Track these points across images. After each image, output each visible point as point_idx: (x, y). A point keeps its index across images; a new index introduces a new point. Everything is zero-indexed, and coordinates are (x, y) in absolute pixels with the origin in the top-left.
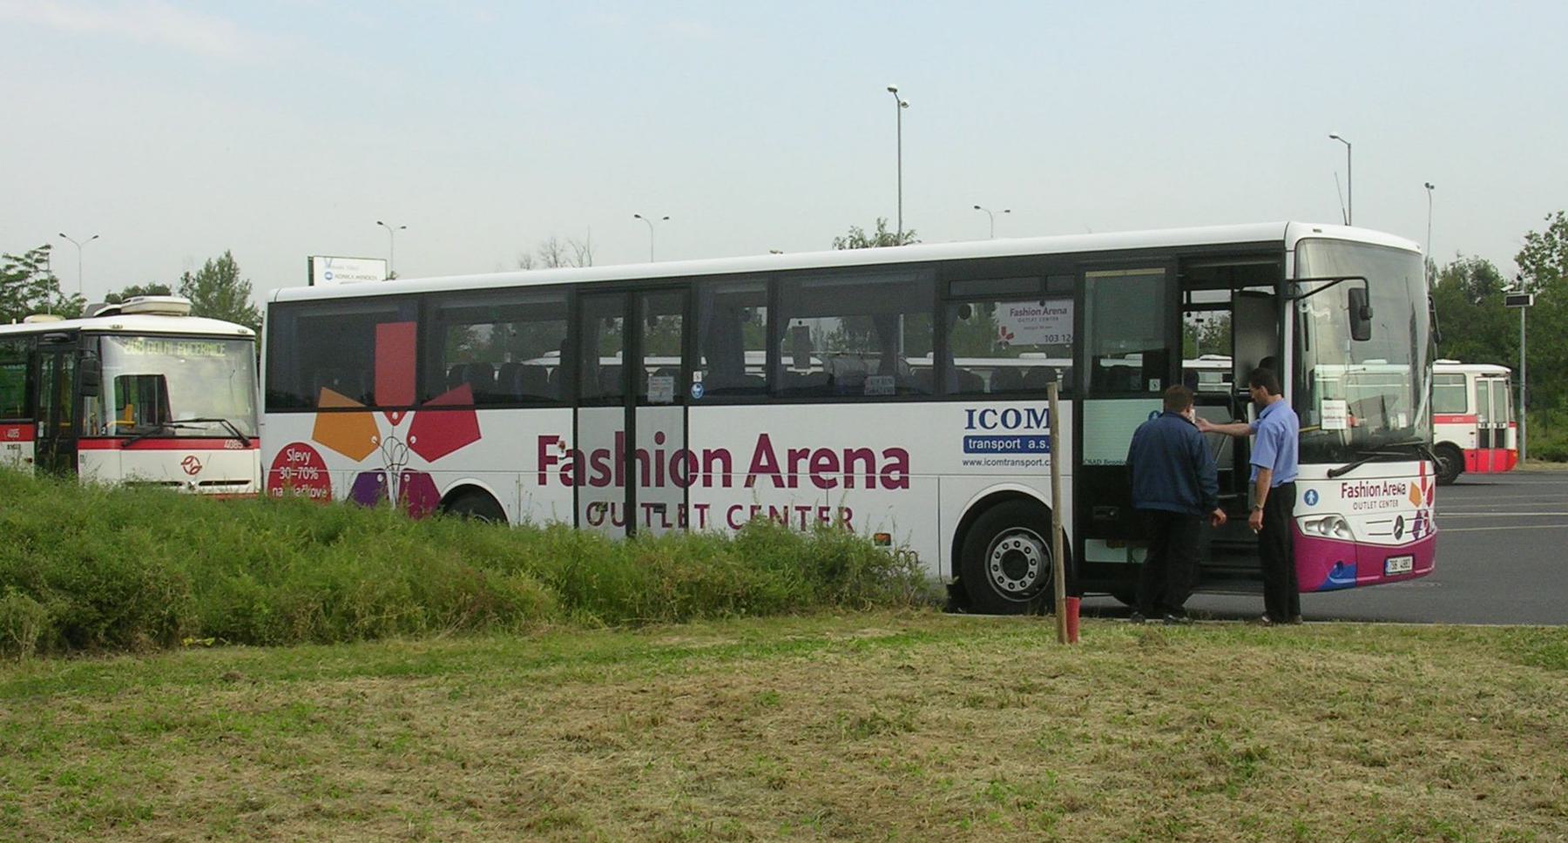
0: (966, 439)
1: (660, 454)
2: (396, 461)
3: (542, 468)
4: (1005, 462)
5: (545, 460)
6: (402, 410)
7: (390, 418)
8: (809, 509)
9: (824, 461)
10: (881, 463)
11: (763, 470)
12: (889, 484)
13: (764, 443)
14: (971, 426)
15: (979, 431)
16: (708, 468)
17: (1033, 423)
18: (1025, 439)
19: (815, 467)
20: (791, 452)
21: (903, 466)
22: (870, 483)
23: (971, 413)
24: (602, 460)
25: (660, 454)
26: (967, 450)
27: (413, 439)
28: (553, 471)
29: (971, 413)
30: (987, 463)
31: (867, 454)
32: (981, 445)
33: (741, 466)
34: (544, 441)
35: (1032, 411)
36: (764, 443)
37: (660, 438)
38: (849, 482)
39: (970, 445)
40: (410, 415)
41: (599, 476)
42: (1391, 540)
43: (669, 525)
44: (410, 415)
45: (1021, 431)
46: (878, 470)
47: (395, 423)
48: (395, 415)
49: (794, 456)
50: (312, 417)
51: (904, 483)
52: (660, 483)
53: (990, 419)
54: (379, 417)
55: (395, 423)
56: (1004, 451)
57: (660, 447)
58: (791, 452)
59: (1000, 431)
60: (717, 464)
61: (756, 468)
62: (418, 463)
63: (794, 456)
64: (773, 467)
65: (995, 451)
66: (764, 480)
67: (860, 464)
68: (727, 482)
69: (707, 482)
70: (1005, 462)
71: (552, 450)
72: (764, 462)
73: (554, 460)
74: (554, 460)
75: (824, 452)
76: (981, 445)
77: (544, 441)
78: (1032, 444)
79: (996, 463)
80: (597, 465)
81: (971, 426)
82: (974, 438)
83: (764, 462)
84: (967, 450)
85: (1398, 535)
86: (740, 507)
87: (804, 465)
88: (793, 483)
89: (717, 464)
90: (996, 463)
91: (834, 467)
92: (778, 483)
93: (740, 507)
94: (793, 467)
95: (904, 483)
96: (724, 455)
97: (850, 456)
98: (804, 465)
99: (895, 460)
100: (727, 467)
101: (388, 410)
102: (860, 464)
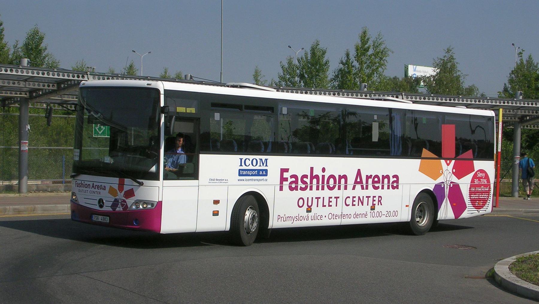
0: (240, 170)
1: (323, 177)
2: (448, 180)
3: (281, 183)
4: (252, 180)
5: (283, 179)
6: (451, 159)
7: (446, 162)
8: (320, 198)
9: (376, 179)
10: (392, 180)
11: (358, 183)
12: (394, 188)
13: (359, 173)
14: (241, 165)
15: (244, 167)
16: (340, 182)
17: (261, 165)
18: (259, 170)
19: (374, 182)
20: (367, 176)
21: (397, 181)
22: (388, 188)
23: (241, 159)
24: (305, 179)
25: (323, 177)
26: (240, 175)
27: (454, 170)
28: (286, 184)
29: (241, 159)
30: (258, 180)
31: (388, 177)
32: (245, 173)
33: (351, 180)
34: (283, 171)
35: (261, 160)
36: (359, 173)
37: (324, 170)
38: (383, 188)
39: (241, 173)
40: (453, 161)
41: (303, 186)
42: (97, 208)
43: (325, 206)
44: (453, 161)
45: (258, 167)
46: (391, 183)
47: (448, 165)
48: (448, 162)
49: (368, 177)
50: (418, 161)
51: (397, 187)
52: (323, 189)
53: (248, 162)
54: (443, 161)
55: (448, 165)
56: (252, 175)
57: (323, 174)
58: (367, 176)
59: (251, 167)
60: (343, 180)
61: (356, 182)
62: (455, 179)
63: (368, 177)
64: (361, 182)
65: (249, 175)
66: (358, 187)
67: (386, 180)
68: (346, 188)
69: (339, 188)
70: (252, 180)
71: (286, 175)
72: (359, 180)
73: (286, 179)
74: (286, 179)
75: (377, 176)
76: (245, 173)
77: (283, 171)
78: (261, 173)
79: (249, 180)
80: (304, 182)
81: (241, 165)
82: (242, 170)
83: (359, 180)
84: (240, 175)
85: (101, 206)
86: (349, 197)
87: (370, 181)
88: (367, 188)
89: (343, 180)
90: (249, 180)
91: (378, 182)
92: (362, 188)
93: (349, 197)
94: (367, 182)
95: (397, 187)
96: (345, 177)
97: (384, 177)
98: (370, 181)
99: (294, 179)
100: (346, 182)
101: (446, 159)
102: (386, 180)
